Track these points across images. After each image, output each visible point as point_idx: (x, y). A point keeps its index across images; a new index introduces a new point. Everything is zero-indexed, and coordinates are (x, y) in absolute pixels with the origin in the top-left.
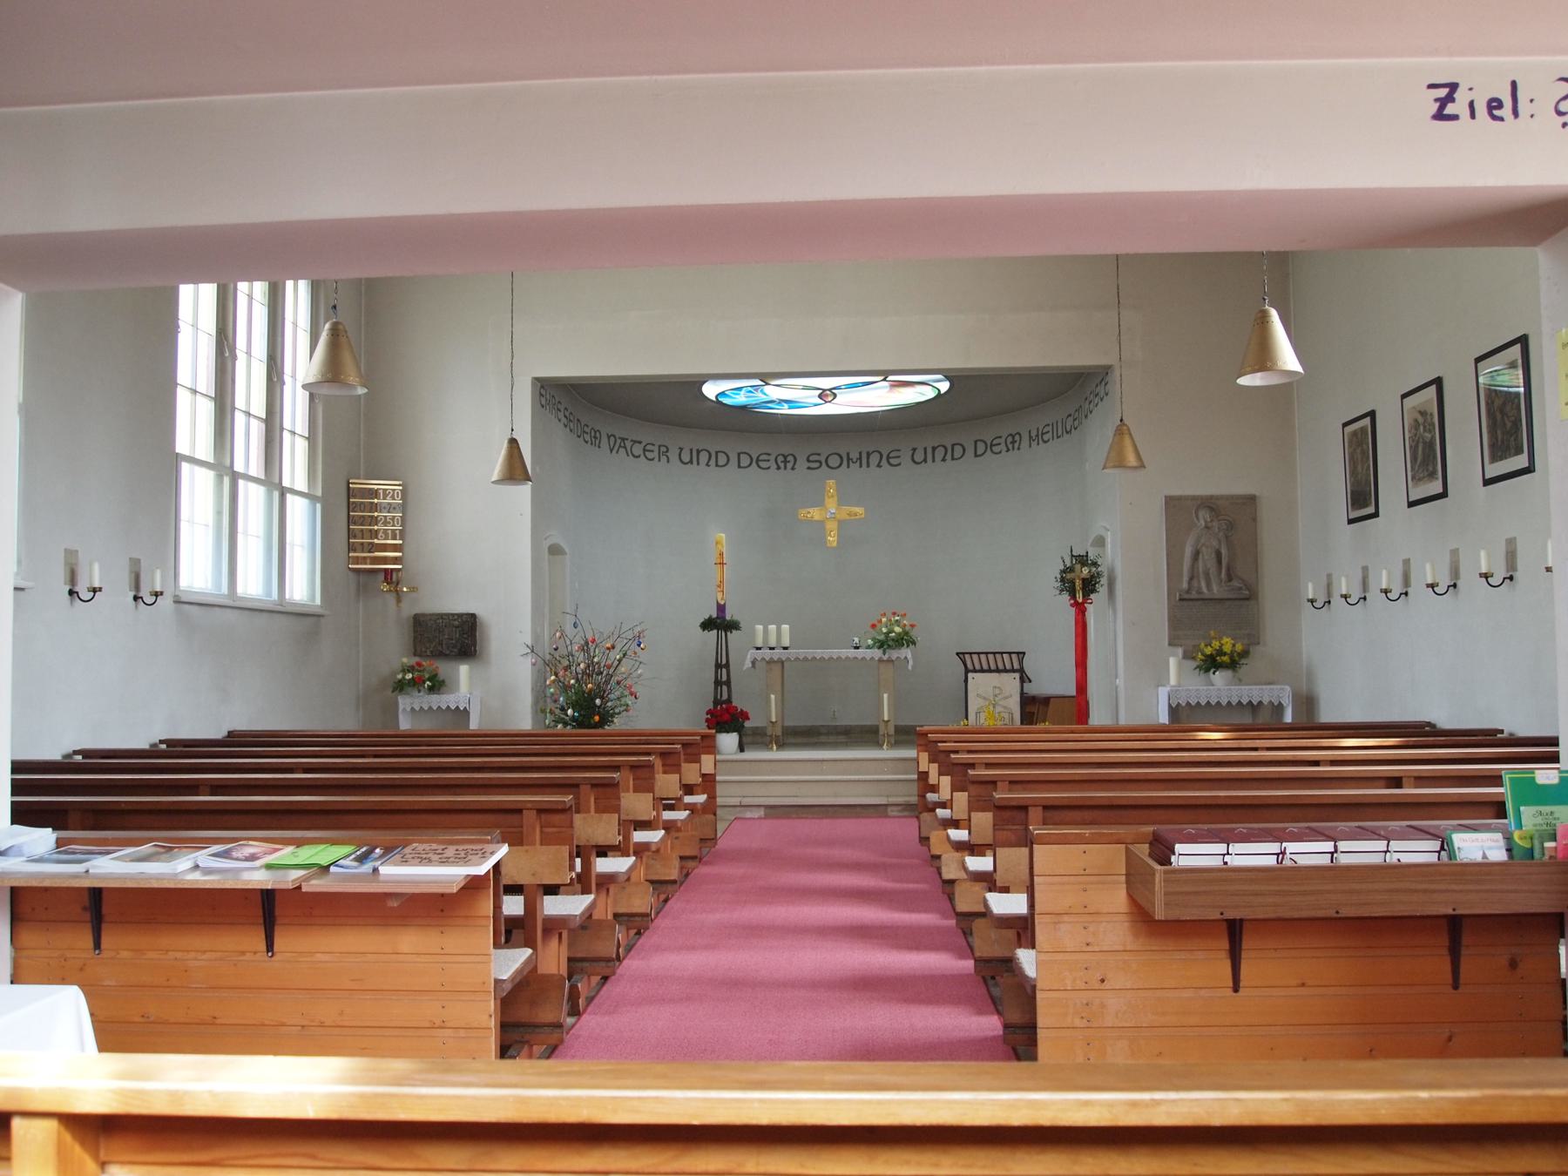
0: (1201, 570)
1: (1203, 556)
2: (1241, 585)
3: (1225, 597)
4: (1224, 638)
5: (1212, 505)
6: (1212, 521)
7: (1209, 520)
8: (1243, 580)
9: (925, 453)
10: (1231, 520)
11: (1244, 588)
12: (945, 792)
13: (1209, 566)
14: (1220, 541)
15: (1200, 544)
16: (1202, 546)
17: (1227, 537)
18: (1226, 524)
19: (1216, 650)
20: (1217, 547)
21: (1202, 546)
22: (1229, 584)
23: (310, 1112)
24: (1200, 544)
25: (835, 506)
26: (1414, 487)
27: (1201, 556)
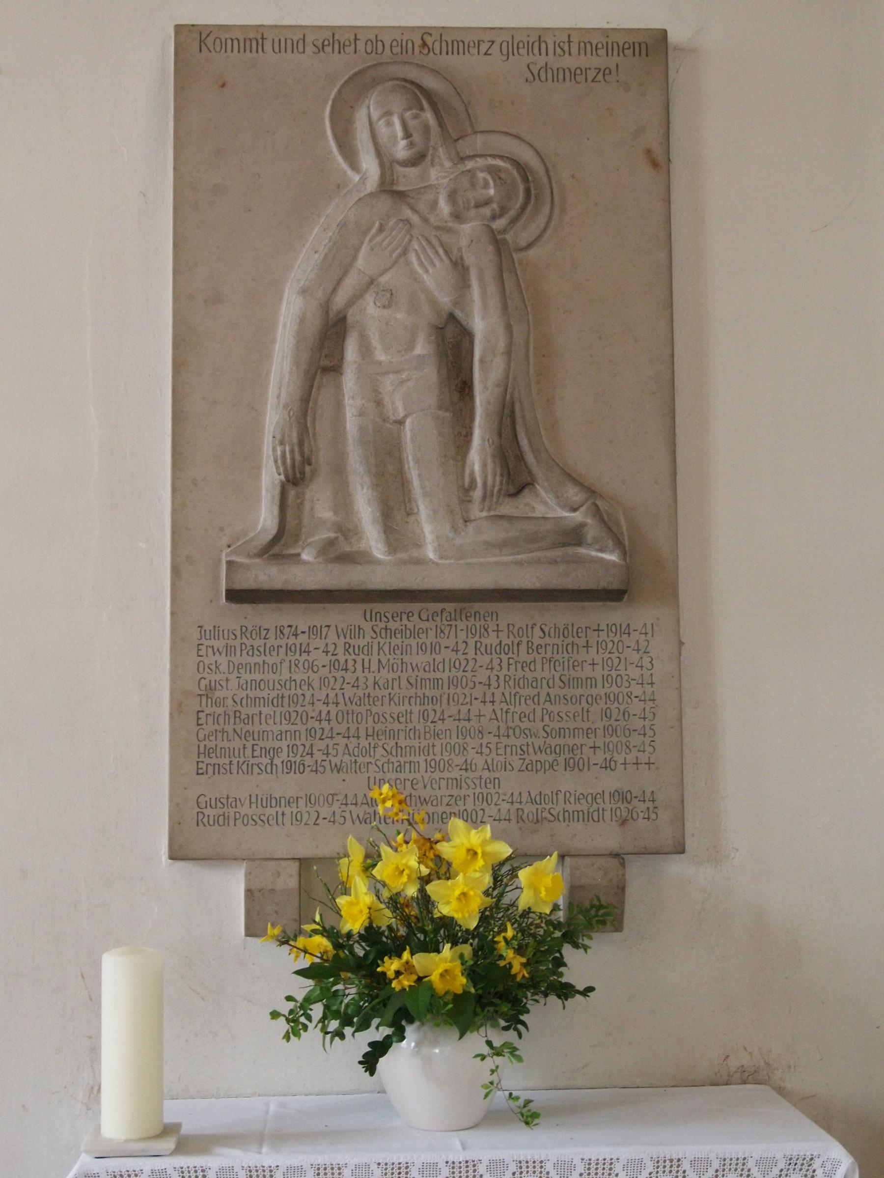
0: (351, 424)
1: (366, 350)
2: (578, 517)
3: (485, 580)
4: (457, 825)
5: (431, 83)
6: (417, 160)
7: (401, 151)
8: (591, 492)
9: (558, 78)
10: (527, 156)
11: (593, 530)
12: (226, 811)
13: (396, 406)
14: (460, 268)
15: (351, 283)
16: (357, 297)
17: (498, 244)
18: (493, 171)
19: (395, 903)
20: (445, 300)
21: (357, 297)
22: (508, 507)
23: (592, 586)
24: (351, 283)
25: (356, 175)
26: (297, 943)
27: (351, 352)
